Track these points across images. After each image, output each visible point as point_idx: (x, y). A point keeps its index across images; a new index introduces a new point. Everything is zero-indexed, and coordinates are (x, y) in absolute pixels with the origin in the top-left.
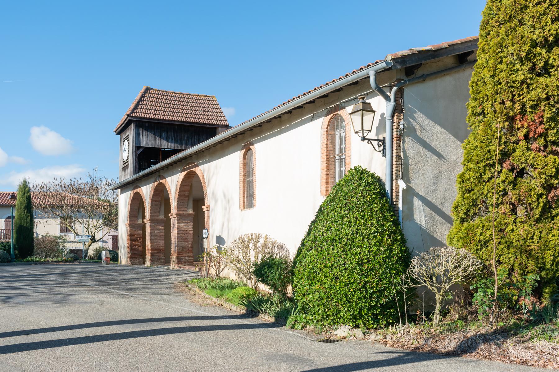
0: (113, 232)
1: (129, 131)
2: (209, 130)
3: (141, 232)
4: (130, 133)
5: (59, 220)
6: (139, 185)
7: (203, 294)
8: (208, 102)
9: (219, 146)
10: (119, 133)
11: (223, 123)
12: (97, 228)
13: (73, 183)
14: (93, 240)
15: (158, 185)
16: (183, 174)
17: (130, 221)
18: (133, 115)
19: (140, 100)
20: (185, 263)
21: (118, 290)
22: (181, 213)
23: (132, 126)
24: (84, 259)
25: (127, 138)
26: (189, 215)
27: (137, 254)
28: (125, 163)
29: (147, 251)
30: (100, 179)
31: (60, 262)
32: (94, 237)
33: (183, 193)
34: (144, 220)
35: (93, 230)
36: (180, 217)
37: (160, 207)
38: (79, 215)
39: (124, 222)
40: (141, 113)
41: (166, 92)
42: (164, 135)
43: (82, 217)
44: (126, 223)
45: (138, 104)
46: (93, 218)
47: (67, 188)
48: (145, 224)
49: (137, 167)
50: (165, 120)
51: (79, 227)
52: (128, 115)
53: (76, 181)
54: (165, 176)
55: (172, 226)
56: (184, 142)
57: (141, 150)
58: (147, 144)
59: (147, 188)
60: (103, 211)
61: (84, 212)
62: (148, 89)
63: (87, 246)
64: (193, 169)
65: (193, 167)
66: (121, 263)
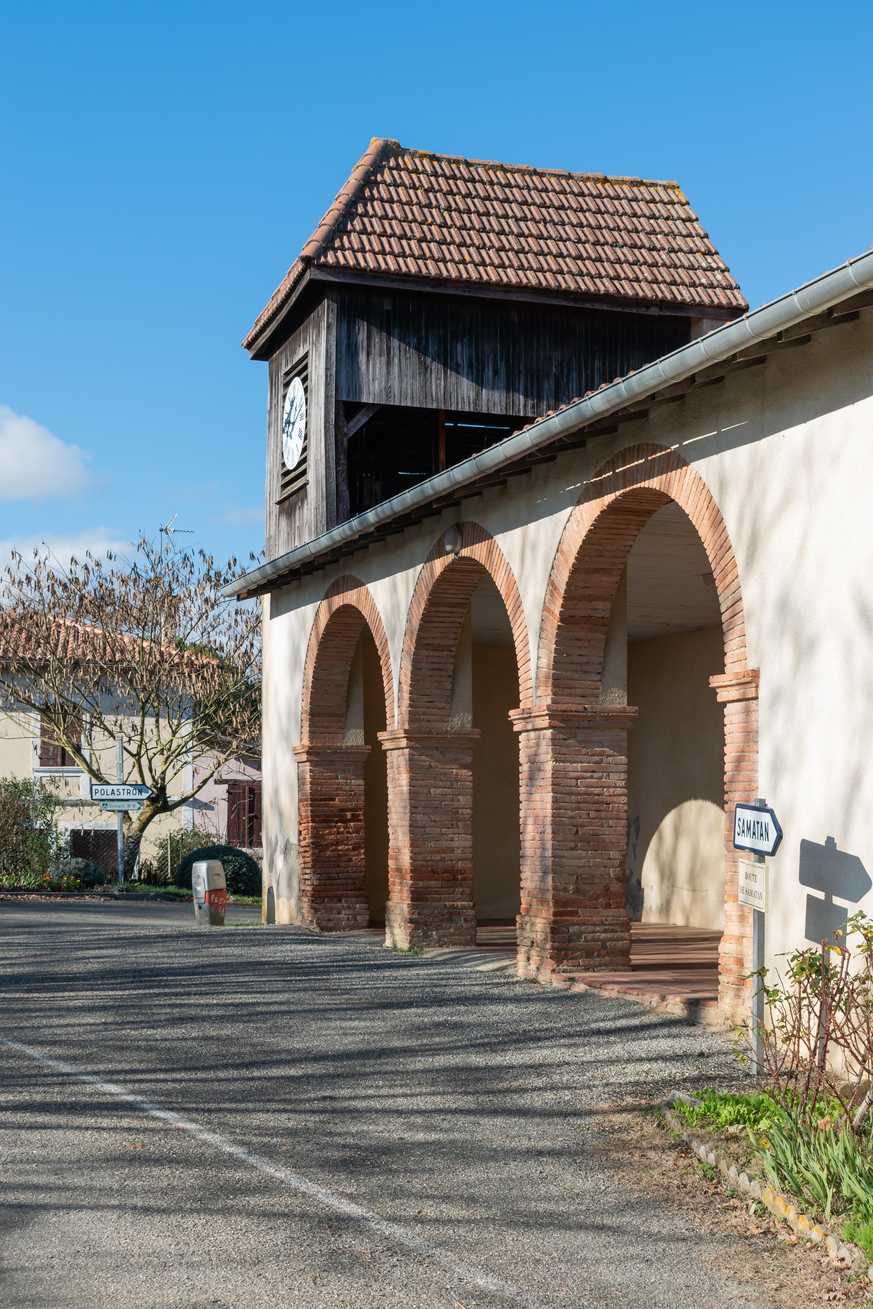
0: (235, 770)
1: (312, 336)
2: (672, 325)
3: (358, 784)
4: (316, 348)
5: (33, 721)
6: (354, 573)
7: (837, 1252)
8: (641, 208)
9: (825, 338)
10: (264, 353)
11: (721, 297)
12: (171, 754)
13: (81, 575)
14: (160, 802)
15: (448, 570)
16: (589, 512)
17: (313, 735)
18: (331, 259)
19: (358, 197)
20: (589, 954)
21: (298, 1162)
22: (572, 706)
23: (325, 313)
24: (121, 884)
25: (301, 370)
26: (610, 719)
27: (345, 880)
28: (293, 481)
29: (392, 877)
30: (186, 558)
31: (28, 890)
32: (162, 789)
33: (582, 609)
34: (381, 736)
35: (158, 763)
36: (568, 725)
37: (453, 677)
38: (103, 700)
39: (285, 736)
40: (360, 253)
41: (468, 164)
42: (462, 353)
43: (116, 710)
44: (296, 743)
45: (349, 212)
46: (157, 716)
47: (59, 590)
48: (383, 754)
49: (346, 493)
50: (469, 283)
51: (105, 750)
52: (307, 261)
53: (91, 565)
54: (486, 524)
55: (524, 768)
56: (548, 385)
57: (361, 420)
58: (388, 391)
59: (394, 588)
60: (196, 688)
61: (122, 691)
62: (389, 151)
63: (136, 825)
64: (654, 483)
65: (650, 472)
66: (271, 919)
